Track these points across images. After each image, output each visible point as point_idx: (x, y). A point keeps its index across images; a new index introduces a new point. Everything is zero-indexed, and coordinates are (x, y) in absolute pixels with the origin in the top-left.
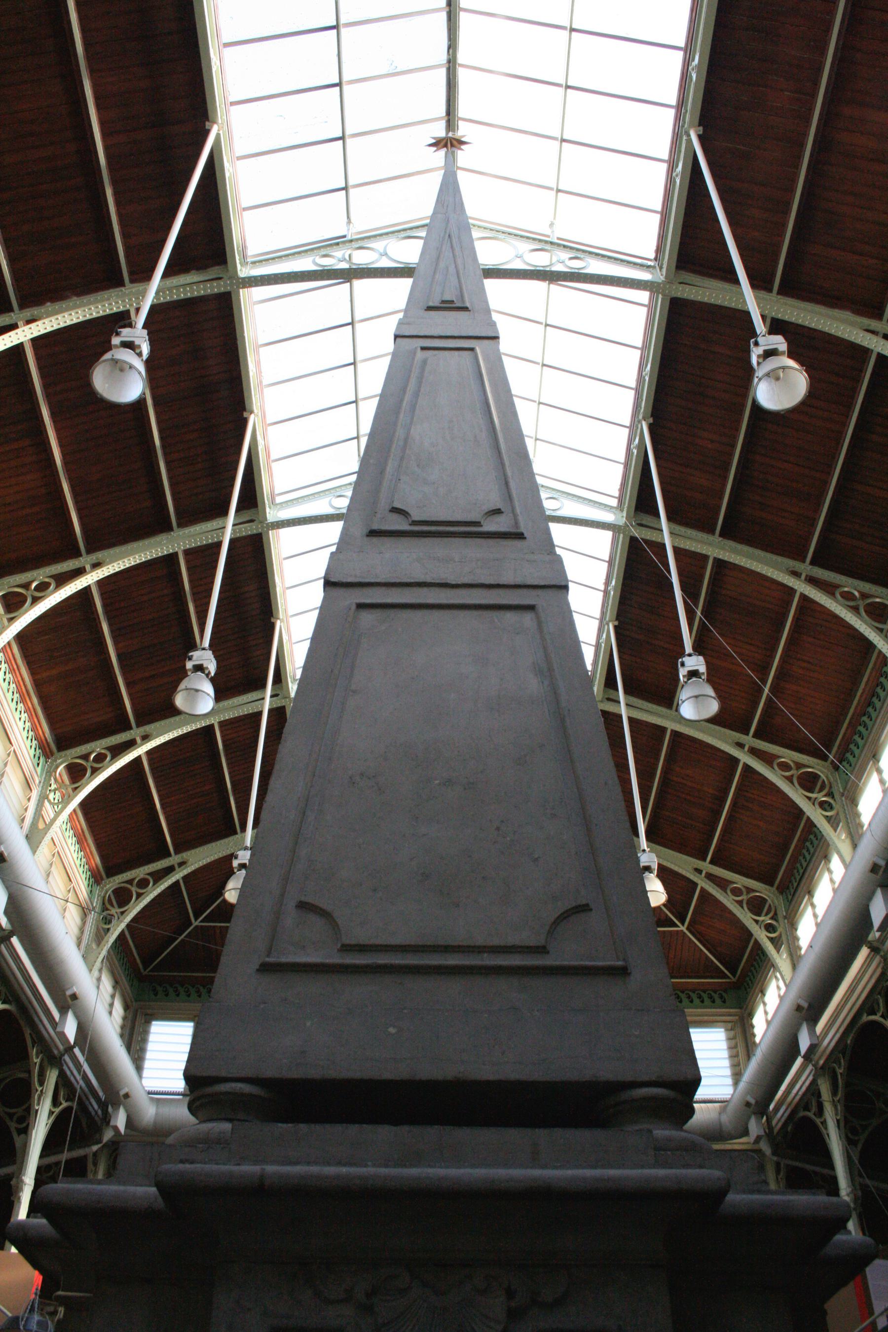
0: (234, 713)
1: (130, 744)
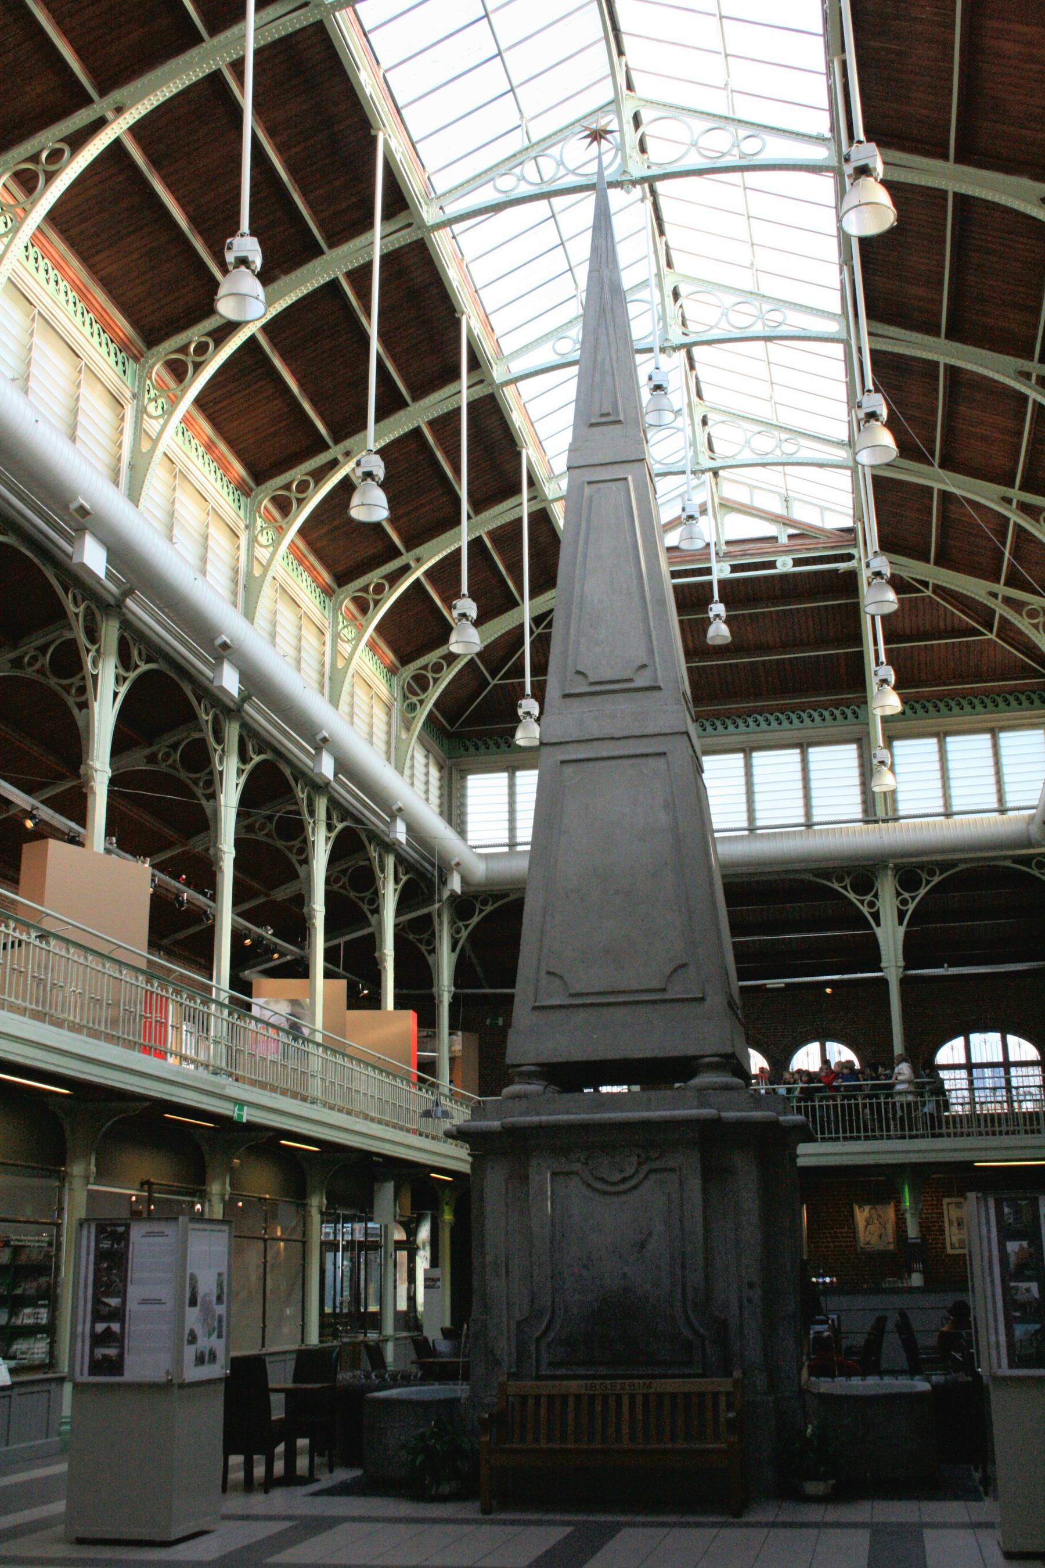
0: (442, 409)
1: (406, 569)
